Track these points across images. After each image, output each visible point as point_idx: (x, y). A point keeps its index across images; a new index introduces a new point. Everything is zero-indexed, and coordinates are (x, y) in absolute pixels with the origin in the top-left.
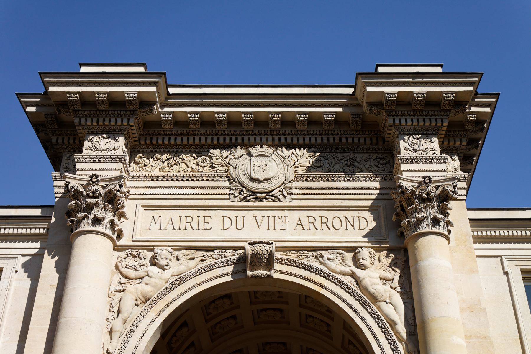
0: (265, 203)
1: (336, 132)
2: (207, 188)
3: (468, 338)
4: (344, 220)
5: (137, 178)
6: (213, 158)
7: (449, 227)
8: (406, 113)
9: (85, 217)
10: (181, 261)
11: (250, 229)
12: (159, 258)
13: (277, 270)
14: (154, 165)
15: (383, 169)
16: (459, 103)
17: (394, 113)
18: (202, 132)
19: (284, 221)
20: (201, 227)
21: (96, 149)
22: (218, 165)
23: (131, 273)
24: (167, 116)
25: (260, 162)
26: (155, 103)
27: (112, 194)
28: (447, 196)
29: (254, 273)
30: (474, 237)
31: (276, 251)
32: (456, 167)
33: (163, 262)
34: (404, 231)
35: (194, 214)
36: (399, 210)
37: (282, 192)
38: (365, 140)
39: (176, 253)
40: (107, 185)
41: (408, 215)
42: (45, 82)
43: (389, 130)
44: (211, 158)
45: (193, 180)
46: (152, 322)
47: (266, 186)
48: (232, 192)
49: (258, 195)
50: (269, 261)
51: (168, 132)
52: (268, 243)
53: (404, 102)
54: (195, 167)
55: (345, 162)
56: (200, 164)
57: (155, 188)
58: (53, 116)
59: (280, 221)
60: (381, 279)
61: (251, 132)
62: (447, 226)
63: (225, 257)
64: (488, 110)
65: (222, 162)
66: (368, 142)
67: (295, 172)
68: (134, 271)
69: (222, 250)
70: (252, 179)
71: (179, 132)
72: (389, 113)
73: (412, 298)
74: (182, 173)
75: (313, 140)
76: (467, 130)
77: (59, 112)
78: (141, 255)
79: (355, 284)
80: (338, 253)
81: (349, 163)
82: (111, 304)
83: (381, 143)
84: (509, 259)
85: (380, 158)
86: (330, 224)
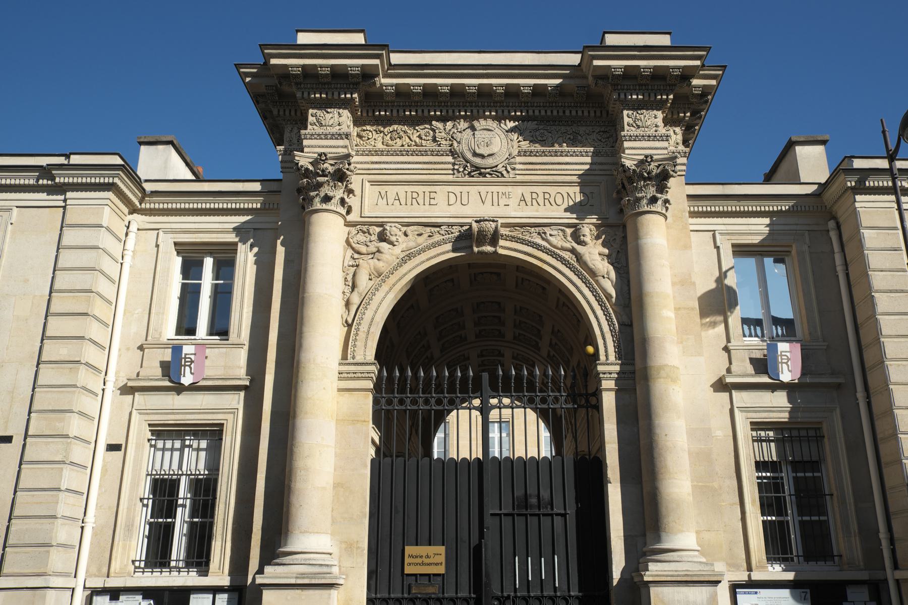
0: (489, 178)
2: (431, 163)
3: (677, 309)
4: (565, 196)
9: (317, 195)
10: (410, 237)
11: (472, 204)
14: (376, 138)
16: (686, 75)
20: (427, 202)
21: (321, 125)
23: (363, 249)
29: (480, 249)
30: (690, 212)
33: (393, 239)
35: (420, 189)
36: (620, 187)
44: (434, 131)
47: (490, 162)
48: (456, 167)
49: (483, 170)
50: (494, 239)
52: (493, 221)
53: (631, 74)
54: (418, 140)
56: (424, 137)
57: (380, 163)
64: (714, 82)
66: (592, 114)
70: (475, 154)
72: (615, 87)
73: (628, 273)
74: (406, 147)
75: (537, 113)
76: (692, 103)
77: (280, 84)
83: (604, 115)
84: (165, 232)
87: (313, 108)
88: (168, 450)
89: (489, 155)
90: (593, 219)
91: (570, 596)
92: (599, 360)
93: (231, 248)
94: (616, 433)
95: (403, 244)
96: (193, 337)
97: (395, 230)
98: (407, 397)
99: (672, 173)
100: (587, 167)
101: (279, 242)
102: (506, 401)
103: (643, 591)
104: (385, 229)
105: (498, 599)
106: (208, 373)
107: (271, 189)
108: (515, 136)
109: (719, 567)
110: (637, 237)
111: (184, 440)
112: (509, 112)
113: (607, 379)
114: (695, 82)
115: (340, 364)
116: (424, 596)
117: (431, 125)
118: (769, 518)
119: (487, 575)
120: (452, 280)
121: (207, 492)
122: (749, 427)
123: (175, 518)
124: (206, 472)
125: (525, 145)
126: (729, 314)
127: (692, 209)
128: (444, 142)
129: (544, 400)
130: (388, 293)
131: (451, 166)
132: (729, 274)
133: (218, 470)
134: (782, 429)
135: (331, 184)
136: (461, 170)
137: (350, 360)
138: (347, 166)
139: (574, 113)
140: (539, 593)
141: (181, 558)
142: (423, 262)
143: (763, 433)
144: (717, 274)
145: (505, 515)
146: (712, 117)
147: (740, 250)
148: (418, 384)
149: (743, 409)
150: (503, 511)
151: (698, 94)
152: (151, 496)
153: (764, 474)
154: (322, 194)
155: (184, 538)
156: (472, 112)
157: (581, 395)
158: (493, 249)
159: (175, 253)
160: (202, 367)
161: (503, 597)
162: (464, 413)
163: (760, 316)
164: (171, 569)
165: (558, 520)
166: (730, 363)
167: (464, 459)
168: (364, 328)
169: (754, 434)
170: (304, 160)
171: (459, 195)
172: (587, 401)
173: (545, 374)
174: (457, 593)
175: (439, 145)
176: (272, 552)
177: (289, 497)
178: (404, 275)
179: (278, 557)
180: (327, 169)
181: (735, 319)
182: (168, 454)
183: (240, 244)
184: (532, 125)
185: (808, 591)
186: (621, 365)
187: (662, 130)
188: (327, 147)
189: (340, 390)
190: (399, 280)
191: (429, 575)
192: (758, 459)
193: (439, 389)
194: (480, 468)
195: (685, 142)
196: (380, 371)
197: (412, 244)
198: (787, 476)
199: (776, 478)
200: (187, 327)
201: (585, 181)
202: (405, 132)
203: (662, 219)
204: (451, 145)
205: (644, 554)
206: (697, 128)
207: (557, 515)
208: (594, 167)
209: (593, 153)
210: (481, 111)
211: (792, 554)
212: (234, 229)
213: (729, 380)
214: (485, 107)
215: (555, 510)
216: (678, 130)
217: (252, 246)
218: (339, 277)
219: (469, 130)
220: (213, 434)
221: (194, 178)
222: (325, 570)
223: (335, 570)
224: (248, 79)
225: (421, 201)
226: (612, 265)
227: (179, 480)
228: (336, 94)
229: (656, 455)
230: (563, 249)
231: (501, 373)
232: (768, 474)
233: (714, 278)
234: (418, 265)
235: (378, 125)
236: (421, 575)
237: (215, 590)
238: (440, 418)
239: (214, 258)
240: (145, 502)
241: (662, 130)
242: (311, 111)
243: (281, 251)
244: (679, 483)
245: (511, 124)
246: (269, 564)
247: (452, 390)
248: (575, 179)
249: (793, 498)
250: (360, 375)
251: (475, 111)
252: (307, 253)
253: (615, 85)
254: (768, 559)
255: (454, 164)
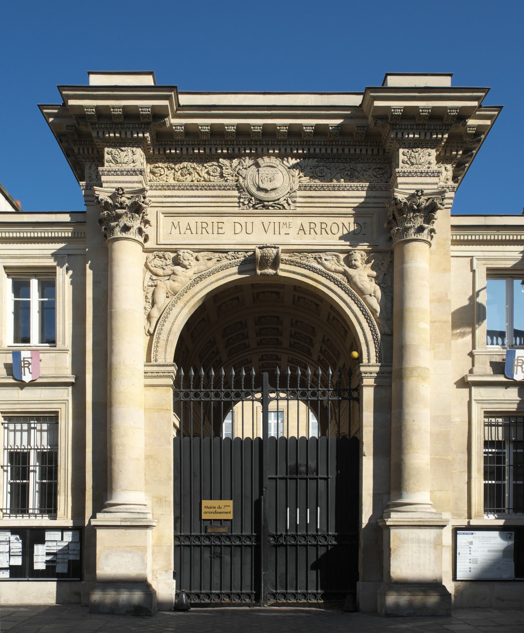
0: (271, 210)
1: (340, 143)
2: (219, 197)
3: (432, 322)
4: (341, 226)
5: (228, 187)
6: (224, 168)
7: (433, 234)
8: (409, 127)
9: (117, 225)
10: (201, 261)
11: (256, 233)
12: (182, 259)
13: (282, 269)
14: (167, 174)
15: (380, 179)
16: (463, 115)
17: (397, 127)
18: (212, 143)
19: (288, 226)
21: (117, 162)
22: (228, 174)
23: (160, 272)
24: (179, 127)
25: (267, 172)
26: (167, 116)
27: (138, 205)
28: (435, 207)
29: (263, 271)
30: (453, 241)
31: (282, 252)
32: (449, 177)
33: (186, 263)
34: (393, 237)
36: (391, 218)
37: (287, 200)
38: (367, 150)
39: (195, 254)
40: (132, 197)
41: (398, 223)
42: (63, 96)
43: (391, 143)
44: (221, 167)
45: (206, 190)
46: (181, 310)
47: (273, 195)
48: (242, 200)
49: (266, 203)
50: (276, 262)
51: (179, 143)
52: (275, 248)
53: (409, 115)
54: (206, 176)
55: (346, 172)
56: (212, 173)
57: (172, 197)
58: (74, 128)
59: (285, 227)
60: (368, 276)
61: (258, 143)
62: (431, 233)
63: (238, 258)
64: (488, 122)
65: (232, 172)
66: (370, 152)
67: (300, 182)
68: (162, 270)
69: (235, 252)
70: (259, 189)
71: (190, 143)
72: (393, 126)
73: (392, 292)
74: (196, 183)
75: (318, 151)
78: (167, 257)
79: (346, 280)
80: (334, 255)
81: (349, 173)
82: (146, 296)
83: (381, 152)
85: (379, 168)
86: (328, 230)
87: (108, 147)
88: (18, 431)
89: (273, 190)
90: (365, 246)
91: (328, 535)
92: (362, 362)
93: (51, 271)
94: (372, 419)
95: (195, 268)
96: (28, 345)
97: (187, 256)
98: (201, 392)
99: (439, 206)
100: (362, 200)
101: (88, 265)
102: (282, 395)
103: (385, 532)
104: (178, 255)
105: (273, 536)
106: (43, 372)
107: (79, 220)
108: (296, 172)
109: (446, 516)
110: (403, 261)
111: (29, 424)
112: (292, 150)
113: (368, 377)
114: (471, 122)
115: (145, 366)
116: (217, 534)
117: (218, 162)
118: (490, 482)
119: (265, 521)
120: (238, 298)
121: (51, 462)
122: (483, 415)
123: (29, 479)
124: (49, 447)
125: (306, 180)
126: (477, 326)
127: (454, 238)
128: (230, 178)
129: (314, 394)
130: (183, 308)
131: (236, 200)
132: (481, 293)
133: (57, 445)
134: (510, 417)
135: (129, 215)
136: (246, 202)
137: (153, 363)
138: (142, 200)
139: (352, 151)
140: (305, 533)
141: (36, 507)
142: (213, 283)
143: (493, 420)
144: (471, 293)
145: (280, 478)
146: (483, 155)
147: (494, 273)
148: (210, 381)
149: (478, 401)
150: (278, 476)
151: (471, 134)
152: (9, 464)
153: (490, 450)
154: (122, 225)
155: (37, 494)
156: (256, 150)
157: (346, 390)
158: (274, 272)
159: (6, 275)
160: (38, 368)
161: (277, 535)
162: (248, 404)
163: (503, 329)
164: (30, 515)
165: (321, 483)
166: (473, 365)
167: (248, 438)
168: (164, 336)
169: (486, 420)
170: (103, 194)
171: (244, 225)
172: (350, 394)
173: (315, 375)
174: (242, 532)
175: (226, 181)
176: (101, 503)
177: (111, 465)
178: (197, 293)
179: (106, 507)
180: (124, 202)
181: (481, 331)
182: (18, 434)
183: (58, 268)
184: (312, 162)
185: (513, 533)
186: (381, 366)
187: (434, 167)
188: (123, 182)
189: (146, 386)
190: (192, 297)
191: (220, 520)
192: (487, 439)
193: (227, 385)
194: (260, 445)
195: (455, 178)
196: (178, 371)
197: (202, 267)
198: (508, 452)
199: (500, 453)
200: (22, 335)
201: (359, 213)
202: (194, 169)
203: (426, 246)
204: (237, 181)
205: (388, 507)
206: (467, 165)
207: (321, 479)
208: (368, 200)
209: (369, 187)
210: (265, 150)
211: (504, 507)
212: (53, 255)
213: (470, 379)
214: (269, 146)
215: (320, 475)
216: (449, 167)
217: (68, 269)
218: (141, 295)
219: (254, 167)
220: (51, 419)
221: (14, 210)
222: (141, 516)
223: (149, 516)
224: (51, 120)
225: (210, 230)
226: (379, 285)
227: (29, 453)
228: (129, 133)
229: (403, 435)
230: (336, 271)
231: (279, 372)
232: (494, 450)
233: (468, 297)
234: (208, 285)
235: (169, 162)
236: (214, 520)
237: (63, 529)
238: (229, 407)
239: (39, 279)
240: (5, 468)
241: (434, 167)
242: (106, 149)
243: (89, 273)
244: (421, 455)
245: (293, 161)
246: (100, 512)
247: (238, 385)
248: (350, 211)
249: (512, 468)
250: (162, 374)
251: (259, 149)
252: (112, 276)
253: (393, 125)
254: (485, 511)
255: (240, 198)
